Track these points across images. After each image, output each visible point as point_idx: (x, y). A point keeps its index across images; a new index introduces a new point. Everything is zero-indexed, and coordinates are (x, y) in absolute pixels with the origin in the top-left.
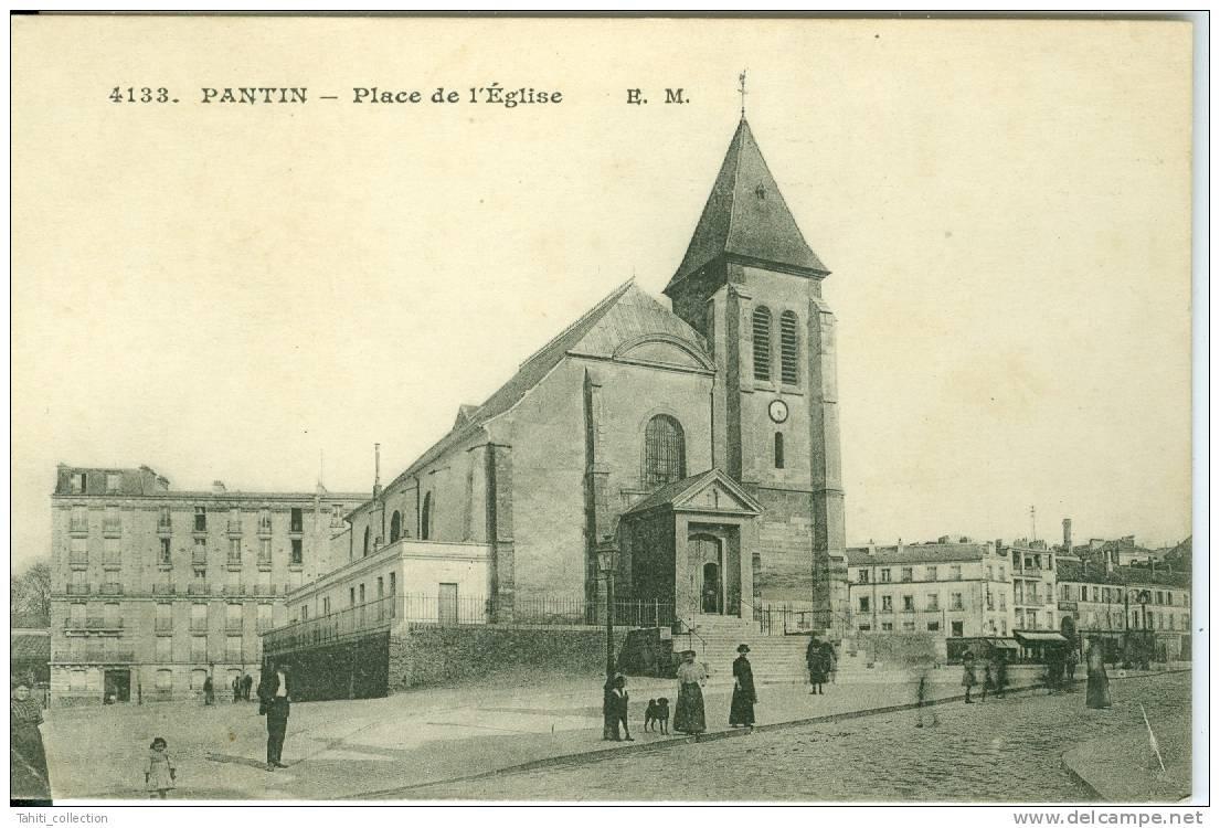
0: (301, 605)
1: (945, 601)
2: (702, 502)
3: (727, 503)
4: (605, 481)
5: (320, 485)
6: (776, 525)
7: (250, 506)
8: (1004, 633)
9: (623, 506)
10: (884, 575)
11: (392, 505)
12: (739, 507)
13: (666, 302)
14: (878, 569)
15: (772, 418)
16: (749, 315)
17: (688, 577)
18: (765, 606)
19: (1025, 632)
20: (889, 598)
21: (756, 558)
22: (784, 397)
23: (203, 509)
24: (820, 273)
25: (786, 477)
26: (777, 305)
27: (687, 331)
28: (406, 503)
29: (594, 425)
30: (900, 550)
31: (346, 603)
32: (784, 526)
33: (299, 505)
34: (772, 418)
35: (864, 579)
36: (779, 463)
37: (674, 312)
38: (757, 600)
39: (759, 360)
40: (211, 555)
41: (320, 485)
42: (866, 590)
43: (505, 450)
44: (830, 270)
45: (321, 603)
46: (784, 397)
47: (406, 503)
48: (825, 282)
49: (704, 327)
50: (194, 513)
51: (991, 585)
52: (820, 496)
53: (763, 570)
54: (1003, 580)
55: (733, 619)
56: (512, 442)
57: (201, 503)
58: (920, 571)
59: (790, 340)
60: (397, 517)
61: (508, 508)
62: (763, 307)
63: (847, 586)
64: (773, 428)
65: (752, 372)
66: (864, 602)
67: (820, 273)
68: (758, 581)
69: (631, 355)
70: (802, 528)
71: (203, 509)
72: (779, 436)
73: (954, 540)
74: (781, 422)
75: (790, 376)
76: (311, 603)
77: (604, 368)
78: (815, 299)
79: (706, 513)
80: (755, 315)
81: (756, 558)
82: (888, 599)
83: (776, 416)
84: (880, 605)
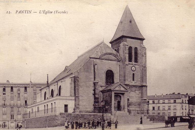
0: (37, 107)
1: (167, 108)
2: (117, 89)
3: (122, 89)
4: (97, 84)
5: (31, 82)
6: (132, 93)
7: (15, 86)
8: (186, 115)
9: (101, 89)
10: (158, 102)
11: (52, 87)
12: (125, 89)
13: (110, 45)
14: (157, 100)
15: (132, 70)
16: (128, 48)
17: (114, 103)
18: (130, 109)
19: (191, 115)
20: (159, 107)
21: (128, 99)
22: (135, 66)
23: (5, 87)
24: (142, 39)
25: (135, 83)
26: (133, 47)
27: (114, 52)
28: (55, 88)
29: (95, 72)
30: (162, 96)
31: (43, 109)
32: (134, 93)
33: (26, 86)
34: (132, 70)
35: (154, 102)
36: (133, 80)
37: (112, 47)
38: (128, 108)
39: (131, 60)
40: (7, 97)
41: (31, 82)
42: (154, 105)
43: (77, 78)
44: (145, 38)
45: (37, 108)
46: (135, 66)
47: (55, 88)
48: (144, 41)
49: (117, 51)
50: (3, 88)
51: (183, 104)
52: (142, 87)
53: (130, 102)
54: (186, 103)
55: (171, 107)
56: (79, 76)
57: (5, 85)
58: (161, 101)
59: (136, 53)
60: (52, 91)
61: (78, 90)
62: (131, 47)
63: (147, 105)
64: (132, 72)
65: (128, 60)
66: (154, 108)
67: (142, 39)
68: (128, 104)
69: (103, 58)
70: (138, 93)
71: (5, 87)
72: (133, 74)
73: (176, 93)
74: (135, 71)
75: (136, 61)
76: (34, 108)
77: (98, 60)
78: (142, 45)
79: (118, 91)
80: (129, 48)
81: (128, 99)
82: (159, 107)
83: (133, 70)
84: (157, 109)
